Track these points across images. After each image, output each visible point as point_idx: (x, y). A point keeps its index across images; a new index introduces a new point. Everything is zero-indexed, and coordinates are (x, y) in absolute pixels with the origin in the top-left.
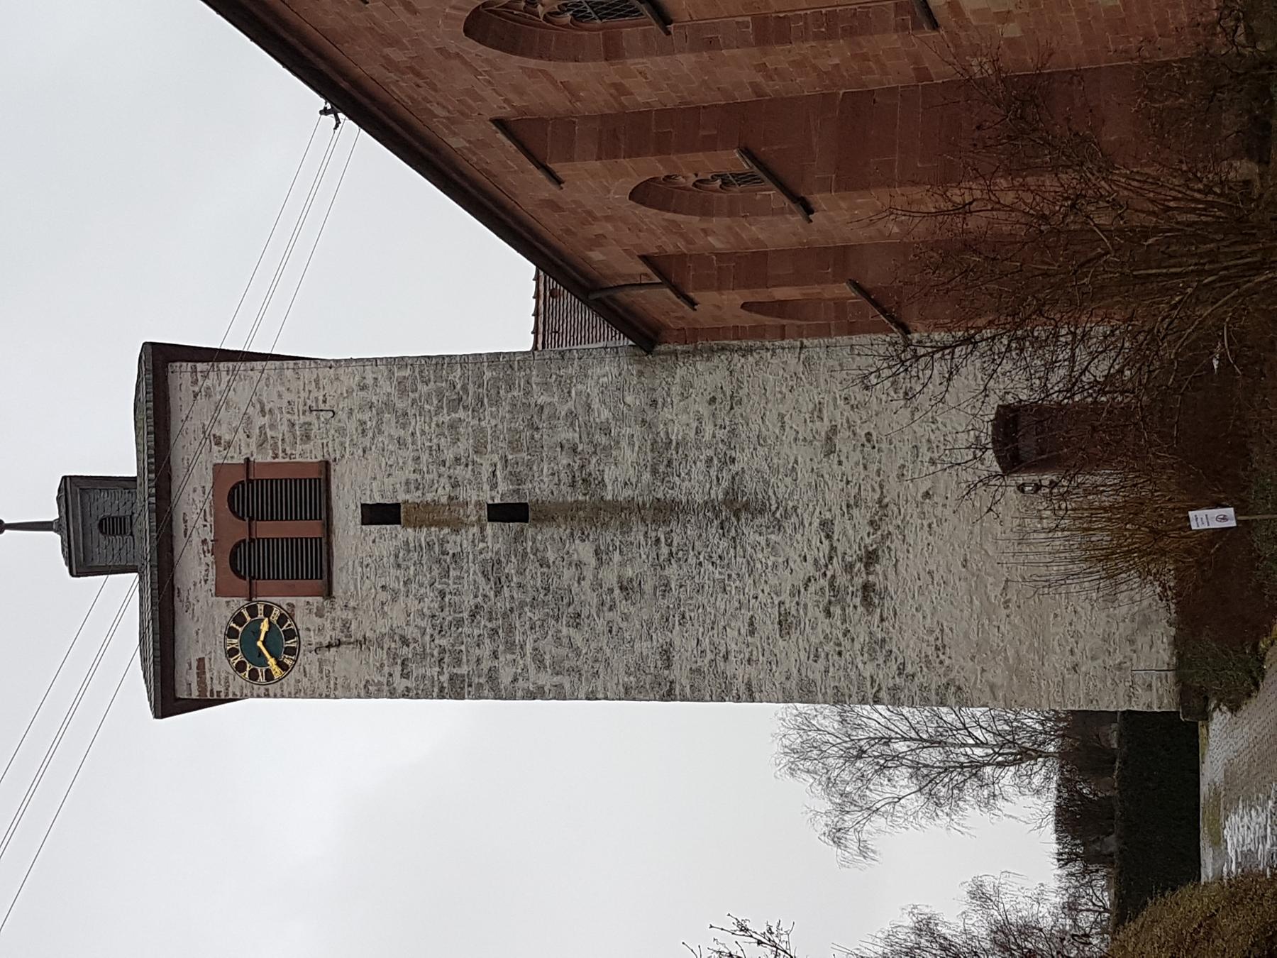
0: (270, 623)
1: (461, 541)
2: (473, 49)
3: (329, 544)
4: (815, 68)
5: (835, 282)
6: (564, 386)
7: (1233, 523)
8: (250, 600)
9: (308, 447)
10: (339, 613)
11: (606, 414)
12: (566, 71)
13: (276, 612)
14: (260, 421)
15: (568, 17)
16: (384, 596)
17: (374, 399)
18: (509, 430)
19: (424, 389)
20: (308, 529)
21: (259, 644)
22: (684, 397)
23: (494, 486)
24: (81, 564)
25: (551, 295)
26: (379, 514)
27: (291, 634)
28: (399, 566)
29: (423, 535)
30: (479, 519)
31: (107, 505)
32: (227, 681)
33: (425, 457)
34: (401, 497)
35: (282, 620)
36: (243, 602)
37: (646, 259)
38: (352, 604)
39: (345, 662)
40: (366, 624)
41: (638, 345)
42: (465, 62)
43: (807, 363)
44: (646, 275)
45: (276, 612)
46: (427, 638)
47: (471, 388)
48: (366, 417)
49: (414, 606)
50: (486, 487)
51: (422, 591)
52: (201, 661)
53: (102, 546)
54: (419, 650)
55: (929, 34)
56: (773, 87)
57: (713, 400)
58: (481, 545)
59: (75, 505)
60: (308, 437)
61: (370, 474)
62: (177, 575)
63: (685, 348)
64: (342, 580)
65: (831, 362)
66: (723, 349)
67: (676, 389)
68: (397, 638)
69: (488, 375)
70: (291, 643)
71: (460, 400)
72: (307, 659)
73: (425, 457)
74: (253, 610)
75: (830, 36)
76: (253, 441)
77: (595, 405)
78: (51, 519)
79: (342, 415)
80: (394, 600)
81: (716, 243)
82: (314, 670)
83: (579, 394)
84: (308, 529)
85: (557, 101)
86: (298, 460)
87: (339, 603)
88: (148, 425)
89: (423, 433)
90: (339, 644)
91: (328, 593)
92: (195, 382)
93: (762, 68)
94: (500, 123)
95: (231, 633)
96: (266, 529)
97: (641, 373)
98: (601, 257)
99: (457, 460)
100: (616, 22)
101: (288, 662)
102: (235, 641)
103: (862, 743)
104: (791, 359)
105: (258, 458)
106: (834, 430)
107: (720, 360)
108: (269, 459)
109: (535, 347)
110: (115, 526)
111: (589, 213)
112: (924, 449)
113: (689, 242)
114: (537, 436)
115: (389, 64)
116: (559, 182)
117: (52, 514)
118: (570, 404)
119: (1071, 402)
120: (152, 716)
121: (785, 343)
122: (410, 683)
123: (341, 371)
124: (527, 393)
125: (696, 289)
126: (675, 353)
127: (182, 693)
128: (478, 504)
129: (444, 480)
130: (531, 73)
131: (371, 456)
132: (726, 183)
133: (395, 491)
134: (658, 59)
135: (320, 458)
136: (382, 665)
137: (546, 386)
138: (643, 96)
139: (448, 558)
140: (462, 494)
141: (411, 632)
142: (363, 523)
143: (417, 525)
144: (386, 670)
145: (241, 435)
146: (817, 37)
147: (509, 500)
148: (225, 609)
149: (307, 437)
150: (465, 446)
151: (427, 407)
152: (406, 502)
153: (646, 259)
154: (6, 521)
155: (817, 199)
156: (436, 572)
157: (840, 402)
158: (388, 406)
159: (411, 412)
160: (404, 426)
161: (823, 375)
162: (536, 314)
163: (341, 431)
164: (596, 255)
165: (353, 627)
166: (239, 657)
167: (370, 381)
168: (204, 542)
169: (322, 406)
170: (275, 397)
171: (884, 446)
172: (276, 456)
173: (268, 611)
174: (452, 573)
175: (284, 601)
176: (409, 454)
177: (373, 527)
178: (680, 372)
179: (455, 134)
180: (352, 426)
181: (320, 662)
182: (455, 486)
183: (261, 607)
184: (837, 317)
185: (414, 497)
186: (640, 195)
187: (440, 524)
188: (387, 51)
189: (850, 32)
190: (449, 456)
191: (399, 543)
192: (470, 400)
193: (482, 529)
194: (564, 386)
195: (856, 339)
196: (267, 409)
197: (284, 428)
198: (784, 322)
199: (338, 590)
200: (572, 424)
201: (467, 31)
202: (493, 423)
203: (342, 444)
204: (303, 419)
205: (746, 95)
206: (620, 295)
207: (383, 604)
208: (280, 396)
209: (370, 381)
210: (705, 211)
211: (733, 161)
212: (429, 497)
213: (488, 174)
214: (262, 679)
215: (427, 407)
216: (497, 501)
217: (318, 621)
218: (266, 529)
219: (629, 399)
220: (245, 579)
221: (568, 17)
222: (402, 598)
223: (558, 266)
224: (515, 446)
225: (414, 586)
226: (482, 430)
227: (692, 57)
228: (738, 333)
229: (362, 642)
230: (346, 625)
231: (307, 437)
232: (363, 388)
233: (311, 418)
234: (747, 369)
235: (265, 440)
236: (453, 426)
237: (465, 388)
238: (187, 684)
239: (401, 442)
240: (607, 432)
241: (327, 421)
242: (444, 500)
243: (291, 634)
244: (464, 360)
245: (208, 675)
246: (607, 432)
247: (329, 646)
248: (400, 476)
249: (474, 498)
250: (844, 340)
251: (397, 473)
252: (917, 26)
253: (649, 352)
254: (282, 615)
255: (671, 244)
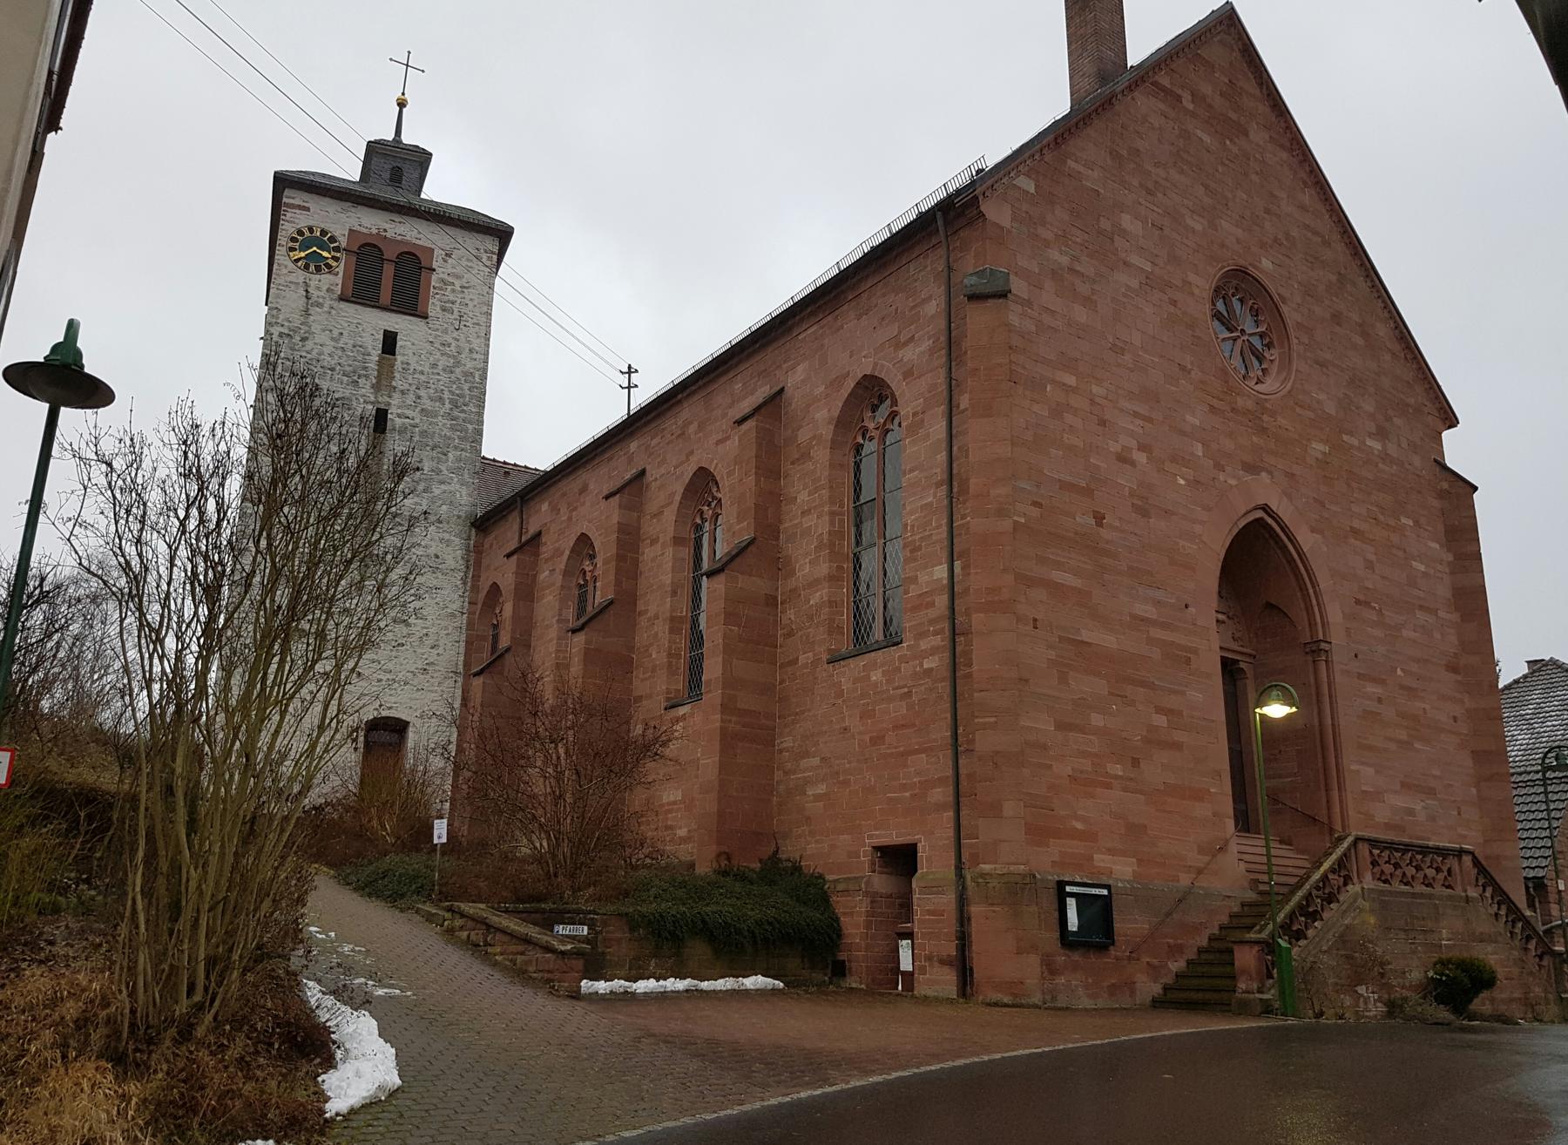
0: (327, 258)
1: (366, 388)
2: (689, 471)
3: (373, 307)
4: (651, 644)
5: (512, 638)
6: (457, 471)
7: (435, 842)
8: (344, 250)
9: (438, 309)
10: (328, 303)
11: (437, 492)
12: (670, 515)
13: (334, 264)
14: (458, 283)
15: (699, 521)
16: (336, 333)
17: (463, 356)
18: (434, 433)
19: (466, 387)
20: (386, 296)
21: (315, 248)
22: (441, 540)
23: (399, 416)
24: (374, 149)
25: (505, 472)
26: (389, 342)
27: (318, 269)
28: (354, 346)
29: (373, 366)
30: (379, 402)
31: (410, 174)
32: (291, 222)
33: (423, 378)
34: (399, 358)
35: (329, 266)
36: (344, 245)
37: (539, 534)
38: (333, 312)
39: (293, 301)
40: (319, 318)
41: (476, 520)
42: (682, 463)
43: (452, 615)
44: (526, 532)
45: (334, 264)
46: (304, 354)
47: (462, 415)
48: (452, 348)
49: (327, 350)
50: (399, 411)
51: (336, 357)
52: (308, 209)
53: (384, 167)
54: (296, 347)
55: (663, 705)
56: (643, 622)
57: (437, 557)
58: (362, 400)
59: (414, 156)
60: (444, 310)
61: (416, 342)
62: (366, 209)
63: (472, 546)
64: (350, 309)
65: (451, 629)
66: (467, 567)
67: (446, 536)
68: (307, 335)
69: (470, 427)
70: (312, 268)
71: (457, 407)
72: (300, 276)
73: (423, 378)
74: (337, 249)
75: (670, 655)
76: (445, 276)
77: (443, 487)
78: (402, 137)
79: (455, 334)
80: (332, 339)
81: (544, 575)
82: (292, 278)
83: (452, 478)
84: (386, 296)
85: (652, 506)
86: (431, 301)
87: (335, 304)
88: (463, 216)
89: (439, 380)
90: (307, 297)
91: (342, 298)
92: (486, 252)
93: (656, 617)
94: (643, 472)
95: (324, 233)
96: (389, 271)
97: (459, 517)
98: (543, 510)
99: (419, 397)
100: (692, 544)
101: (299, 264)
102: (318, 234)
103: (104, 606)
104: (456, 606)
105: (434, 277)
106: (408, 625)
107: (461, 565)
108: (433, 283)
109: (484, 458)
110: (396, 177)
111: (575, 509)
112: (388, 676)
113: (547, 561)
114: (428, 448)
115: (687, 424)
116: (607, 498)
117: (407, 138)
118: (446, 472)
119: (467, 774)
120: (279, 169)
121: (466, 604)
122: (275, 338)
123: (483, 340)
124: (456, 448)
125: (518, 559)
126: (469, 538)
127: (287, 192)
128: (389, 404)
129: (406, 386)
130: (673, 494)
131: (428, 346)
132: (581, 586)
133: (404, 355)
134: (670, 564)
135: (430, 314)
136: (290, 322)
137: (459, 460)
138: (648, 553)
139: (355, 378)
140: (396, 395)
141: (309, 344)
142: (385, 330)
143: (380, 363)
144: (286, 324)
145: (450, 271)
146: (670, 648)
147: (389, 423)
148: (340, 232)
149: (444, 309)
150: (427, 404)
151: (455, 386)
152: (395, 360)
153: (539, 534)
154: (404, 110)
155: (580, 638)
156: (348, 368)
157: (425, 631)
158: (458, 363)
159: (453, 376)
160: (444, 370)
161: (444, 623)
162: (494, 460)
163: (445, 331)
164: (545, 507)
165: (318, 309)
166: (307, 234)
167: (475, 356)
168: (385, 230)
169: (463, 323)
170: (471, 297)
171: (394, 653)
172: (434, 288)
173: (336, 259)
174: (345, 379)
175: (341, 269)
176: (426, 369)
177: (381, 337)
178: (457, 540)
179: (639, 447)
180: (448, 339)
181: (297, 284)
182: (403, 392)
183: (338, 255)
184: (478, 636)
185: (398, 365)
186: (584, 540)
187: (379, 377)
188: (696, 424)
189: (670, 664)
190: (422, 393)
191: (370, 349)
192: (456, 413)
193: (372, 403)
194: (457, 471)
195: (463, 644)
196: (465, 290)
197: (451, 298)
198: (479, 606)
199: (343, 305)
200: (433, 471)
201: (701, 468)
202: (440, 424)
203: (438, 330)
204: (456, 310)
205: (640, 606)
206: (516, 513)
207: (331, 331)
208: (471, 300)
209: (475, 356)
210: (567, 573)
211: (599, 598)
212: (397, 375)
213: (610, 459)
214: (291, 244)
215: (455, 386)
216: (389, 416)
217: (325, 288)
218: (389, 271)
219: (444, 507)
220: (359, 249)
221: (699, 521)
222: (332, 343)
223: (546, 481)
224: (423, 433)
225: (340, 353)
226: (436, 416)
227: (669, 582)
228: (476, 577)
229: (307, 312)
230: (320, 305)
231: (444, 309)
232: (471, 351)
233: (456, 315)
234: (453, 579)
235: (445, 284)
236: (441, 399)
237: (463, 411)
238: (291, 197)
239: (434, 366)
240: (425, 491)
241: (452, 324)
242: (394, 383)
243: (318, 269)
244: (480, 414)
245: (298, 211)
246: (425, 491)
247: (307, 291)
248: (413, 361)
249: (393, 402)
250: (463, 637)
251: (416, 358)
252: (668, 699)
253: (473, 524)
254: (332, 267)
255: (546, 550)
